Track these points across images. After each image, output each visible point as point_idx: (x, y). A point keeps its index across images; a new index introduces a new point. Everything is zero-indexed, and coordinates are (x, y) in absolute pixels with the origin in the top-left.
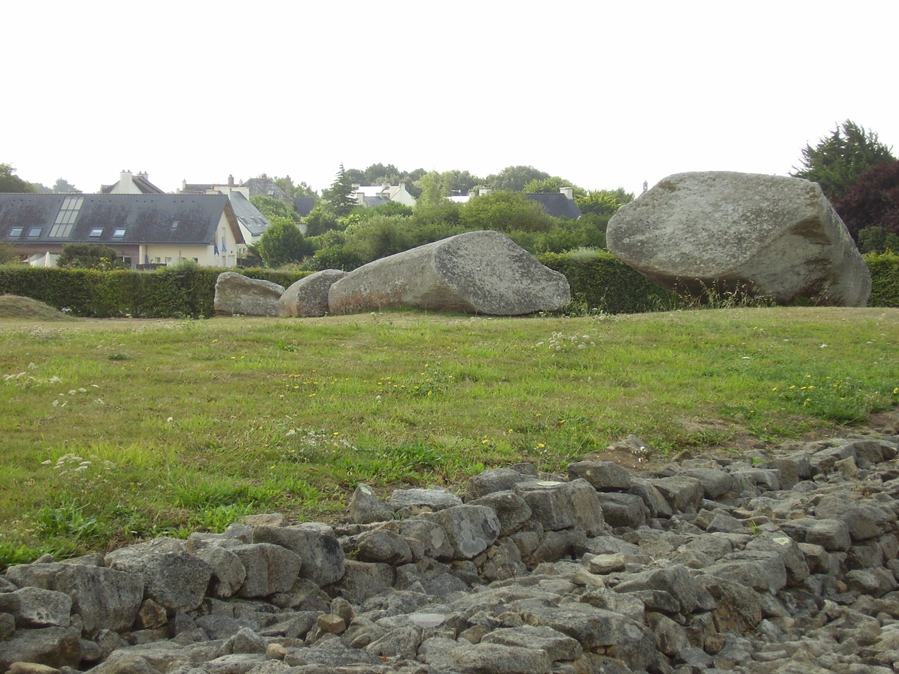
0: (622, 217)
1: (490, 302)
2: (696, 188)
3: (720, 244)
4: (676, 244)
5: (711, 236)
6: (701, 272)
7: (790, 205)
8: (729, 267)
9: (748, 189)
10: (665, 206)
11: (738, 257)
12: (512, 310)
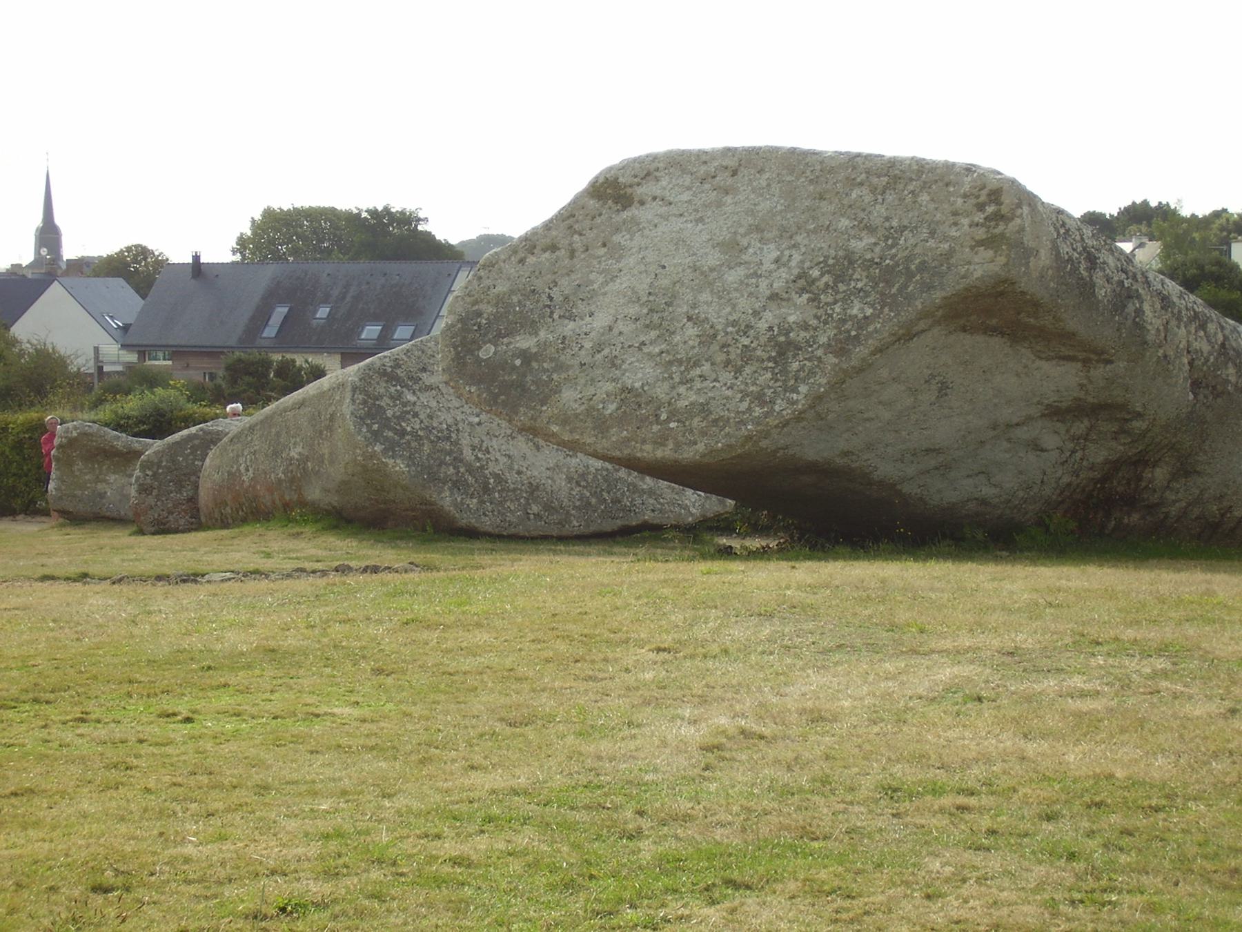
0: (486, 282)
1: (501, 503)
2: (686, 196)
3: (728, 363)
4: (613, 363)
5: (708, 339)
6: (671, 445)
7: (931, 243)
8: (744, 432)
9: (822, 198)
10: (603, 251)
11: (772, 402)
12: (561, 523)
